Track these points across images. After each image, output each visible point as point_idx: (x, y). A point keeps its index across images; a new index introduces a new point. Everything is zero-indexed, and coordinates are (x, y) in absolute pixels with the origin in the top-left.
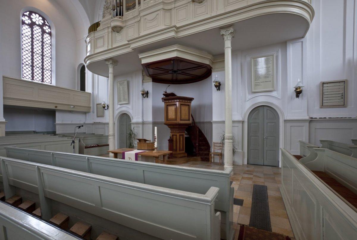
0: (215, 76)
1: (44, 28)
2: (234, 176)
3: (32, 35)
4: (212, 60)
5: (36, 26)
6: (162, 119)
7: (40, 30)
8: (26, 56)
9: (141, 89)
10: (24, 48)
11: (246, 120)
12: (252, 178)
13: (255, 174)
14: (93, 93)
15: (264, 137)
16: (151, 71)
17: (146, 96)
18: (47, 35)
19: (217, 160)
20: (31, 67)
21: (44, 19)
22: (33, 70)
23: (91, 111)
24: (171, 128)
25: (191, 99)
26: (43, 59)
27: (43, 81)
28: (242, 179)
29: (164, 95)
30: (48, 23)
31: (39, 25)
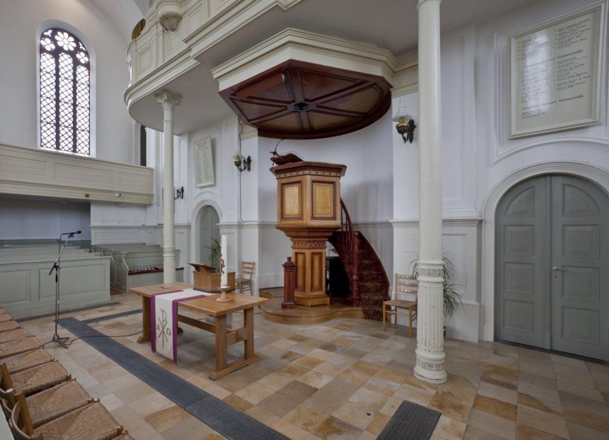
0: (399, 106)
1: (78, 56)
2: (446, 388)
3: (57, 69)
4: (391, 65)
5: (63, 53)
6: (274, 219)
7: (70, 61)
8: (47, 108)
9: (235, 152)
10: (44, 94)
11: (491, 217)
12: (516, 407)
13: (523, 387)
14: (156, 167)
15: (554, 268)
16: (253, 110)
17: (245, 168)
18: (83, 68)
19: (402, 319)
20: (55, 127)
21: (77, 40)
22: (58, 131)
23: (155, 201)
24: (292, 237)
25: (339, 170)
26: (75, 111)
27: (74, 151)
28: (474, 405)
29: (273, 160)
30: (83, 46)
31: (68, 52)
